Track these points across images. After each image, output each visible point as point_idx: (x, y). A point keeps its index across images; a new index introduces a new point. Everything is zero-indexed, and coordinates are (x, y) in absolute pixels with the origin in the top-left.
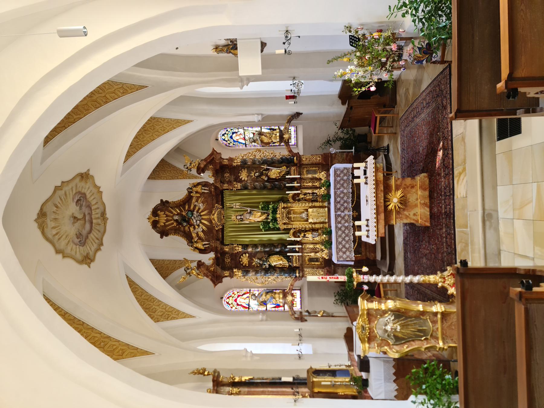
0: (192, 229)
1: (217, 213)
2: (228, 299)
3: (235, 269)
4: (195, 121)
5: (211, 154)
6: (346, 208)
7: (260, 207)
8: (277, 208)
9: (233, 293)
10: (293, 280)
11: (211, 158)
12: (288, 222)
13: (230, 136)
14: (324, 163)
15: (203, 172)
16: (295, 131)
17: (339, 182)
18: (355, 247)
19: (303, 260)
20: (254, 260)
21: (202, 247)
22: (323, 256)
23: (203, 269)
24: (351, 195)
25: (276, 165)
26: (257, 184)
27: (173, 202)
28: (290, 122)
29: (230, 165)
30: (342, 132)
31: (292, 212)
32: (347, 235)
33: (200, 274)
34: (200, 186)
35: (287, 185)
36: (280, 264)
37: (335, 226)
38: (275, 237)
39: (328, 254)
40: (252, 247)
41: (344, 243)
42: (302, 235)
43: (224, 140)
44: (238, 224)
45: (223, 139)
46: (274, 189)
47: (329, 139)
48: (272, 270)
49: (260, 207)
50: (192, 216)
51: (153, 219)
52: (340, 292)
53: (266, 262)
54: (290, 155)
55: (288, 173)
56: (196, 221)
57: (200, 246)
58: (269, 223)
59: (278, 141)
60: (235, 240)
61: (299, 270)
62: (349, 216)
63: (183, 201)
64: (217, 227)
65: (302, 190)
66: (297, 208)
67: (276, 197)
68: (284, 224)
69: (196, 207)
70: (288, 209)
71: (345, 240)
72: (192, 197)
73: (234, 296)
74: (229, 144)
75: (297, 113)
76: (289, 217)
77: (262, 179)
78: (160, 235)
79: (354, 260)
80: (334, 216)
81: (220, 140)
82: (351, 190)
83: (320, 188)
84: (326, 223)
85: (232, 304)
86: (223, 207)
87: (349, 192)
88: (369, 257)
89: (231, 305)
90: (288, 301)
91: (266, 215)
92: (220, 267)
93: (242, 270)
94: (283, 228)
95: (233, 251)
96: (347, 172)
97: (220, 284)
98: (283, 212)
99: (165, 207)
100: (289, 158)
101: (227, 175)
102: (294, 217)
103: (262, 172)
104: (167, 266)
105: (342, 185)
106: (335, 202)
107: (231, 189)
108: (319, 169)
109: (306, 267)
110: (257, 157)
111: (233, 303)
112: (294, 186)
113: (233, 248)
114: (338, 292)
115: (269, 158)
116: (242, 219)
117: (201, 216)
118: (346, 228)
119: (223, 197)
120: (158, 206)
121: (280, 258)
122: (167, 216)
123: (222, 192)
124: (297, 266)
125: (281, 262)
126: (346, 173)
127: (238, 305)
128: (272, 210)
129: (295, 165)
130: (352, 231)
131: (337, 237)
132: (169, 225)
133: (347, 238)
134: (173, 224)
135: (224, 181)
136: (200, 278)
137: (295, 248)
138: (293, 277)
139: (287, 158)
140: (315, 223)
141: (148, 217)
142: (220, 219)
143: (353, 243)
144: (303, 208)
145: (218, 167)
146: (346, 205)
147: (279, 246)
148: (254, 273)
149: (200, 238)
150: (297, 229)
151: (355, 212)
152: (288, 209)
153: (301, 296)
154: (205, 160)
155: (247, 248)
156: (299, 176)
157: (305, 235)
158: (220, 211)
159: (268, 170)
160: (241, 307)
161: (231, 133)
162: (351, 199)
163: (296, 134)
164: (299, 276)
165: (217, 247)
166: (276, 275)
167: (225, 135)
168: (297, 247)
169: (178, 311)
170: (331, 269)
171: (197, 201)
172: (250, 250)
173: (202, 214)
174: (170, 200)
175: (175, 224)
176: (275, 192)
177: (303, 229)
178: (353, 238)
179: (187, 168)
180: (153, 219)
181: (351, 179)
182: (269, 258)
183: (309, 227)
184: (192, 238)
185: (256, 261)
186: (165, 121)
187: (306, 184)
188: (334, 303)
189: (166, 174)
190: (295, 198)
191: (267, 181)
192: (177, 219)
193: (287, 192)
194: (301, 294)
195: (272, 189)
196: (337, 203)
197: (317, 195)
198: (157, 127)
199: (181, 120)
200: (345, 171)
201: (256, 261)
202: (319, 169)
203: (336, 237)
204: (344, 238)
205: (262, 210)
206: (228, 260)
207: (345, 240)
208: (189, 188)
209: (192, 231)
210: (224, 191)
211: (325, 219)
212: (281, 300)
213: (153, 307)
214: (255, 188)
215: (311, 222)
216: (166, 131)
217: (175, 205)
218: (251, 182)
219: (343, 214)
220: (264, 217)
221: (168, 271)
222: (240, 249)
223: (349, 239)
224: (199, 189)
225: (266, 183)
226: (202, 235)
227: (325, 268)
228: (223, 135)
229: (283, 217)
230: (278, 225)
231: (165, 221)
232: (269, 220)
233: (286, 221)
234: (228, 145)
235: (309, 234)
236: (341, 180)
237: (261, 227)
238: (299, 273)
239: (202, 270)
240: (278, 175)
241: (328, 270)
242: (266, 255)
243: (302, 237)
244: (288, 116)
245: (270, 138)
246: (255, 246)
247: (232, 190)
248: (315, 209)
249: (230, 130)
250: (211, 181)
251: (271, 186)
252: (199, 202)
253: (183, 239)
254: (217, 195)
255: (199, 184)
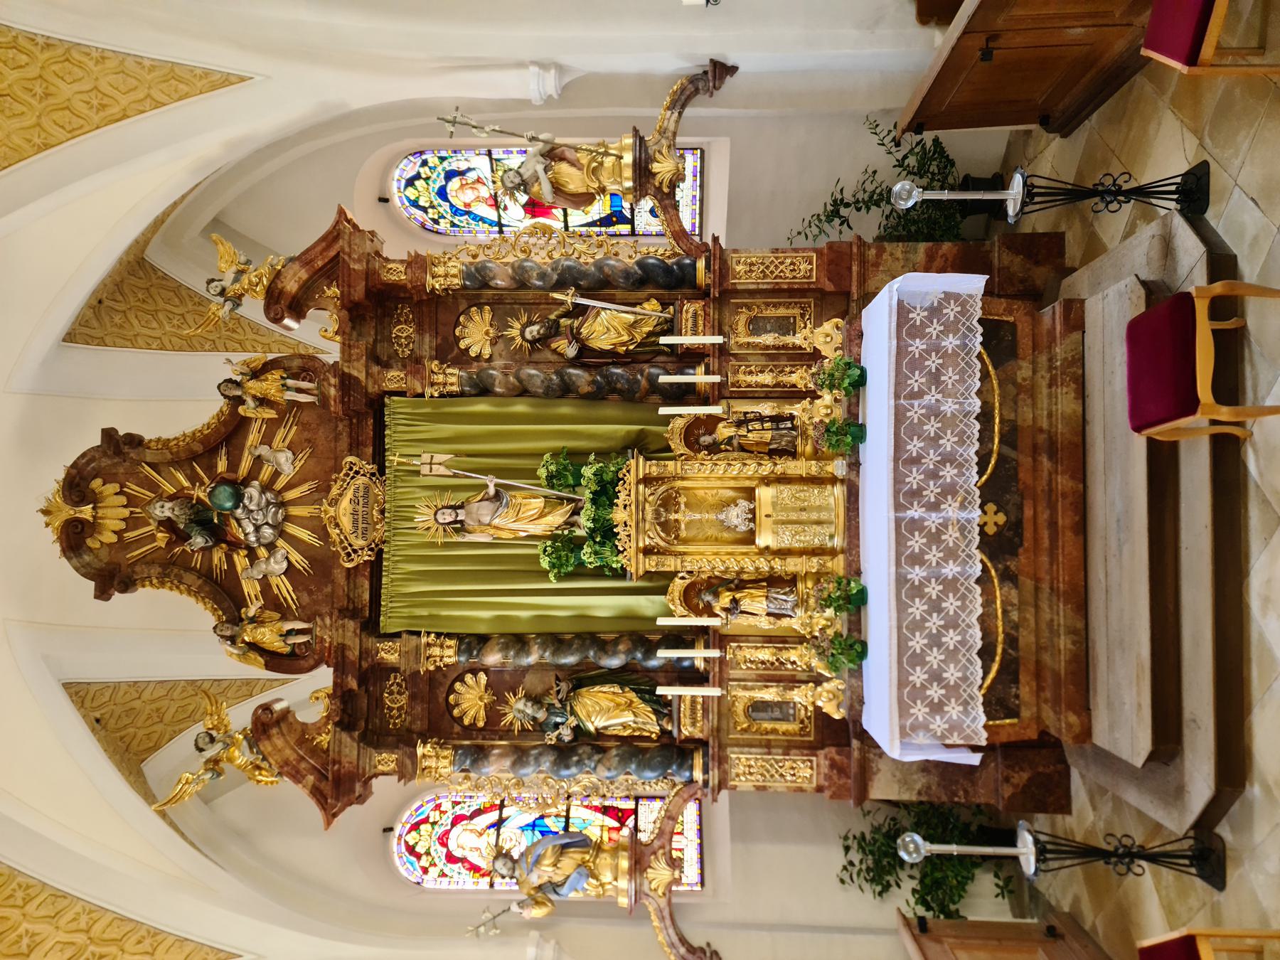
0: (240, 560)
1: (349, 494)
2: (413, 833)
3: (425, 743)
4: (258, 78)
5: (329, 233)
6: (949, 490)
7: (542, 473)
8: (616, 480)
9: (438, 807)
10: (677, 794)
11: (332, 253)
12: (662, 544)
13: (437, 186)
14: (829, 287)
15: (298, 312)
16: (695, 176)
17: (916, 364)
18: (988, 681)
19: (724, 710)
20: (512, 700)
21: (277, 645)
22: (819, 703)
23: (279, 742)
24: (978, 426)
25: (619, 293)
26: (533, 372)
27: (159, 440)
28: (683, 107)
29: (414, 287)
30: (900, 166)
31: (682, 500)
32: (952, 623)
33: (264, 764)
34: (276, 374)
35: (664, 379)
36: (625, 726)
37: (893, 577)
38: (604, 606)
39: (841, 698)
40: (505, 648)
41: (935, 658)
42: (725, 599)
43: (415, 204)
44: (447, 545)
45: (409, 200)
46: (603, 399)
47: (839, 197)
48: (588, 749)
49: (542, 473)
50: (237, 507)
51: (68, 512)
52: (868, 837)
53: (562, 715)
54: (678, 250)
55: (670, 327)
56: (257, 529)
57: (268, 636)
58: (577, 544)
59: (628, 189)
60: (431, 617)
61: (705, 755)
62: (962, 529)
63: (205, 440)
64: (349, 555)
65: (732, 402)
66: (705, 484)
67: (616, 431)
68: (648, 551)
69: (261, 469)
70: (663, 488)
71: (939, 645)
72: (244, 423)
73: (437, 818)
74: (436, 222)
75: (715, 63)
76: (667, 521)
77: (555, 351)
78: (93, 583)
79: (984, 743)
80: (893, 525)
81: (397, 202)
82: (977, 403)
83: (814, 396)
84: (833, 553)
85: (428, 853)
86: (382, 471)
87: (967, 414)
88: (1053, 732)
89: (424, 858)
90: (653, 886)
91: (568, 508)
92: (356, 734)
93: (456, 748)
94: (641, 572)
95: (418, 660)
96: (962, 313)
97: (355, 807)
98: (641, 498)
99: (127, 464)
100: (673, 264)
101: (404, 331)
102: (689, 525)
103: (556, 322)
104: (154, 706)
105: (935, 378)
106: (896, 459)
107: (420, 391)
108: (803, 316)
109: (738, 744)
110: (537, 259)
111: (432, 851)
112: (691, 386)
113: (418, 648)
114: (863, 834)
115: (587, 264)
116: (461, 522)
117: (282, 505)
118: (950, 585)
119: (380, 427)
120: (92, 460)
121: (622, 700)
122: (132, 501)
123: (377, 405)
124: (698, 735)
125: (628, 718)
126: (957, 321)
127: (451, 859)
128: (594, 487)
129: (703, 294)
130: (980, 600)
131: (905, 628)
132: (139, 542)
133: (951, 638)
134: (152, 538)
135: (390, 357)
136: (266, 783)
137: (692, 659)
138: (677, 779)
139: (663, 261)
140: (783, 553)
141: (43, 505)
142: (362, 523)
143: (979, 662)
144: (732, 484)
145: (359, 292)
146: (949, 473)
147: (621, 647)
148: (507, 763)
149: (273, 602)
150: (704, 576)
151: (991, 507)
152: (663, 488)
153: (700, 824)
154: (304, 259)
155: (479, 651)
156: (719, 339)
157: (735, 602)
158: (367, 488)
159: (580, 311)
160: (463, 871)
161: (442, 175)
162: (977, 446)
163: (702, 186)
164: (706, 783)
165: (343, 648)
166: (603, 772)
167: (417, 183)
168: (699, 655)
169: (155, 933)
170: (849, 756)
171: (267, 440)
172: (493, 658)
173: (291, 495)
174: (148, 433)
175: (162, 538)
176: (609, 410)
177: (728, 576)
178: (979, 634)
179: (223, 292)
180: (68, 512)
181: (979, 348)
182: (577, 696)
183: (757, 569)
184: (239, 601)
185: (519, 711)
186: (110, 64)
187: (749, 379)
188: (842, 881)
189: (160, 324)
190: (695, 433)
191: (576, 362)
192: (169, 518)
193: (664, 411)
194: (700, 816)
195: (598, 395)
196: (906, 462)
197: (794, 428)
198: (65, 90)
199: (191, 69)
200: (951, 311)
201: (519, 710)
202: (803, 316)
203: (899, 628)
204: (939, 634)
205: (552, 487)
206: (396, 700)
207: (939, 645)
208: (229, 381)
209: (245, 569)
210: (386, 400)
211: (832, 537)
212: (623, 883)
213: (21, 930)
214: (522, 392)
215: (767, 548)
216: (115, 110)
217: (169, 456)
218: (506, 367)
219: (933, 520)
220: (557, 518)
221: (159, 727)
222: (449, 654)
223: (963, 643)
224: (270, 385)
225: (572, 371)
226: (284, 587)
227: (821, 753)
228: (410, 182)
229: (644, 520)
230: (620, 557)
231: (123, 525)
232: (580, 532)
233: (654, 538)
234: (429, 224)
235: (752, 596)
236: (928, 352)
237: (545, 563)
238: (706, 770)
239: (274, 747)
240: (626, 338)
241: (833, 765)
242: (564, 686)
243: (726, 610)
244: (671, 78)
245: (595, 171)
246: (518, 641)
247: (422, 395)
248: (786, 491)
249: (437, 161)
250: (331, 352)
251: (594, 382)
252: (275, 444)
253: (201, 605)
254: (352, 416)
255: (268, 367)
